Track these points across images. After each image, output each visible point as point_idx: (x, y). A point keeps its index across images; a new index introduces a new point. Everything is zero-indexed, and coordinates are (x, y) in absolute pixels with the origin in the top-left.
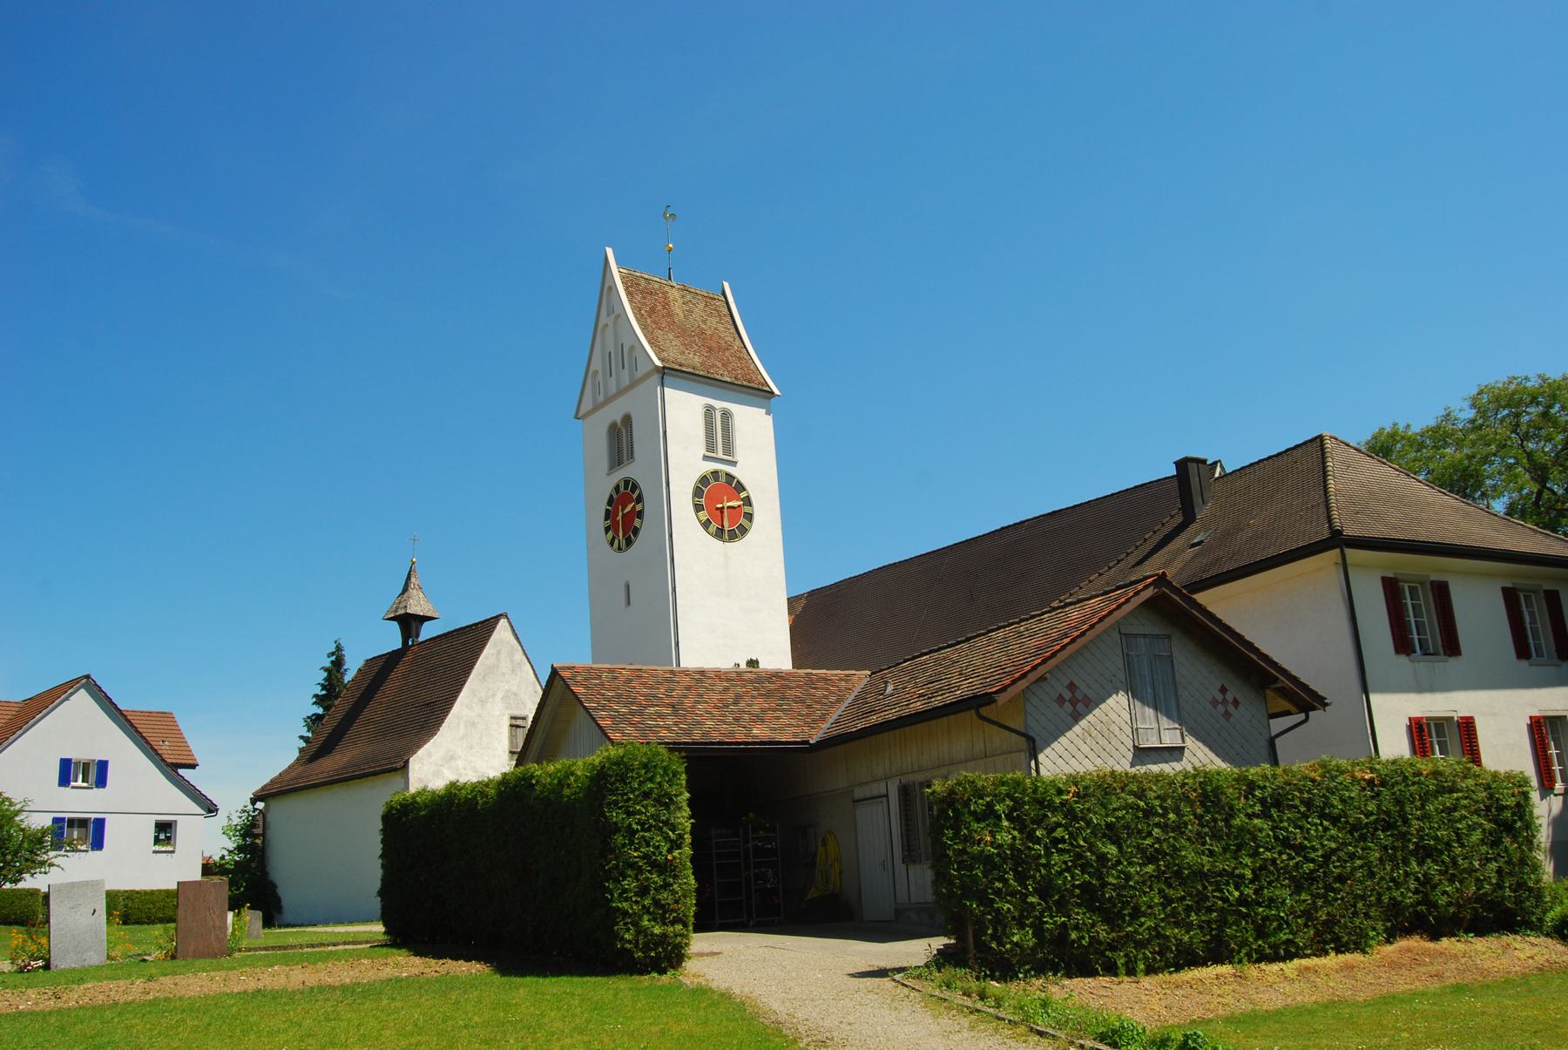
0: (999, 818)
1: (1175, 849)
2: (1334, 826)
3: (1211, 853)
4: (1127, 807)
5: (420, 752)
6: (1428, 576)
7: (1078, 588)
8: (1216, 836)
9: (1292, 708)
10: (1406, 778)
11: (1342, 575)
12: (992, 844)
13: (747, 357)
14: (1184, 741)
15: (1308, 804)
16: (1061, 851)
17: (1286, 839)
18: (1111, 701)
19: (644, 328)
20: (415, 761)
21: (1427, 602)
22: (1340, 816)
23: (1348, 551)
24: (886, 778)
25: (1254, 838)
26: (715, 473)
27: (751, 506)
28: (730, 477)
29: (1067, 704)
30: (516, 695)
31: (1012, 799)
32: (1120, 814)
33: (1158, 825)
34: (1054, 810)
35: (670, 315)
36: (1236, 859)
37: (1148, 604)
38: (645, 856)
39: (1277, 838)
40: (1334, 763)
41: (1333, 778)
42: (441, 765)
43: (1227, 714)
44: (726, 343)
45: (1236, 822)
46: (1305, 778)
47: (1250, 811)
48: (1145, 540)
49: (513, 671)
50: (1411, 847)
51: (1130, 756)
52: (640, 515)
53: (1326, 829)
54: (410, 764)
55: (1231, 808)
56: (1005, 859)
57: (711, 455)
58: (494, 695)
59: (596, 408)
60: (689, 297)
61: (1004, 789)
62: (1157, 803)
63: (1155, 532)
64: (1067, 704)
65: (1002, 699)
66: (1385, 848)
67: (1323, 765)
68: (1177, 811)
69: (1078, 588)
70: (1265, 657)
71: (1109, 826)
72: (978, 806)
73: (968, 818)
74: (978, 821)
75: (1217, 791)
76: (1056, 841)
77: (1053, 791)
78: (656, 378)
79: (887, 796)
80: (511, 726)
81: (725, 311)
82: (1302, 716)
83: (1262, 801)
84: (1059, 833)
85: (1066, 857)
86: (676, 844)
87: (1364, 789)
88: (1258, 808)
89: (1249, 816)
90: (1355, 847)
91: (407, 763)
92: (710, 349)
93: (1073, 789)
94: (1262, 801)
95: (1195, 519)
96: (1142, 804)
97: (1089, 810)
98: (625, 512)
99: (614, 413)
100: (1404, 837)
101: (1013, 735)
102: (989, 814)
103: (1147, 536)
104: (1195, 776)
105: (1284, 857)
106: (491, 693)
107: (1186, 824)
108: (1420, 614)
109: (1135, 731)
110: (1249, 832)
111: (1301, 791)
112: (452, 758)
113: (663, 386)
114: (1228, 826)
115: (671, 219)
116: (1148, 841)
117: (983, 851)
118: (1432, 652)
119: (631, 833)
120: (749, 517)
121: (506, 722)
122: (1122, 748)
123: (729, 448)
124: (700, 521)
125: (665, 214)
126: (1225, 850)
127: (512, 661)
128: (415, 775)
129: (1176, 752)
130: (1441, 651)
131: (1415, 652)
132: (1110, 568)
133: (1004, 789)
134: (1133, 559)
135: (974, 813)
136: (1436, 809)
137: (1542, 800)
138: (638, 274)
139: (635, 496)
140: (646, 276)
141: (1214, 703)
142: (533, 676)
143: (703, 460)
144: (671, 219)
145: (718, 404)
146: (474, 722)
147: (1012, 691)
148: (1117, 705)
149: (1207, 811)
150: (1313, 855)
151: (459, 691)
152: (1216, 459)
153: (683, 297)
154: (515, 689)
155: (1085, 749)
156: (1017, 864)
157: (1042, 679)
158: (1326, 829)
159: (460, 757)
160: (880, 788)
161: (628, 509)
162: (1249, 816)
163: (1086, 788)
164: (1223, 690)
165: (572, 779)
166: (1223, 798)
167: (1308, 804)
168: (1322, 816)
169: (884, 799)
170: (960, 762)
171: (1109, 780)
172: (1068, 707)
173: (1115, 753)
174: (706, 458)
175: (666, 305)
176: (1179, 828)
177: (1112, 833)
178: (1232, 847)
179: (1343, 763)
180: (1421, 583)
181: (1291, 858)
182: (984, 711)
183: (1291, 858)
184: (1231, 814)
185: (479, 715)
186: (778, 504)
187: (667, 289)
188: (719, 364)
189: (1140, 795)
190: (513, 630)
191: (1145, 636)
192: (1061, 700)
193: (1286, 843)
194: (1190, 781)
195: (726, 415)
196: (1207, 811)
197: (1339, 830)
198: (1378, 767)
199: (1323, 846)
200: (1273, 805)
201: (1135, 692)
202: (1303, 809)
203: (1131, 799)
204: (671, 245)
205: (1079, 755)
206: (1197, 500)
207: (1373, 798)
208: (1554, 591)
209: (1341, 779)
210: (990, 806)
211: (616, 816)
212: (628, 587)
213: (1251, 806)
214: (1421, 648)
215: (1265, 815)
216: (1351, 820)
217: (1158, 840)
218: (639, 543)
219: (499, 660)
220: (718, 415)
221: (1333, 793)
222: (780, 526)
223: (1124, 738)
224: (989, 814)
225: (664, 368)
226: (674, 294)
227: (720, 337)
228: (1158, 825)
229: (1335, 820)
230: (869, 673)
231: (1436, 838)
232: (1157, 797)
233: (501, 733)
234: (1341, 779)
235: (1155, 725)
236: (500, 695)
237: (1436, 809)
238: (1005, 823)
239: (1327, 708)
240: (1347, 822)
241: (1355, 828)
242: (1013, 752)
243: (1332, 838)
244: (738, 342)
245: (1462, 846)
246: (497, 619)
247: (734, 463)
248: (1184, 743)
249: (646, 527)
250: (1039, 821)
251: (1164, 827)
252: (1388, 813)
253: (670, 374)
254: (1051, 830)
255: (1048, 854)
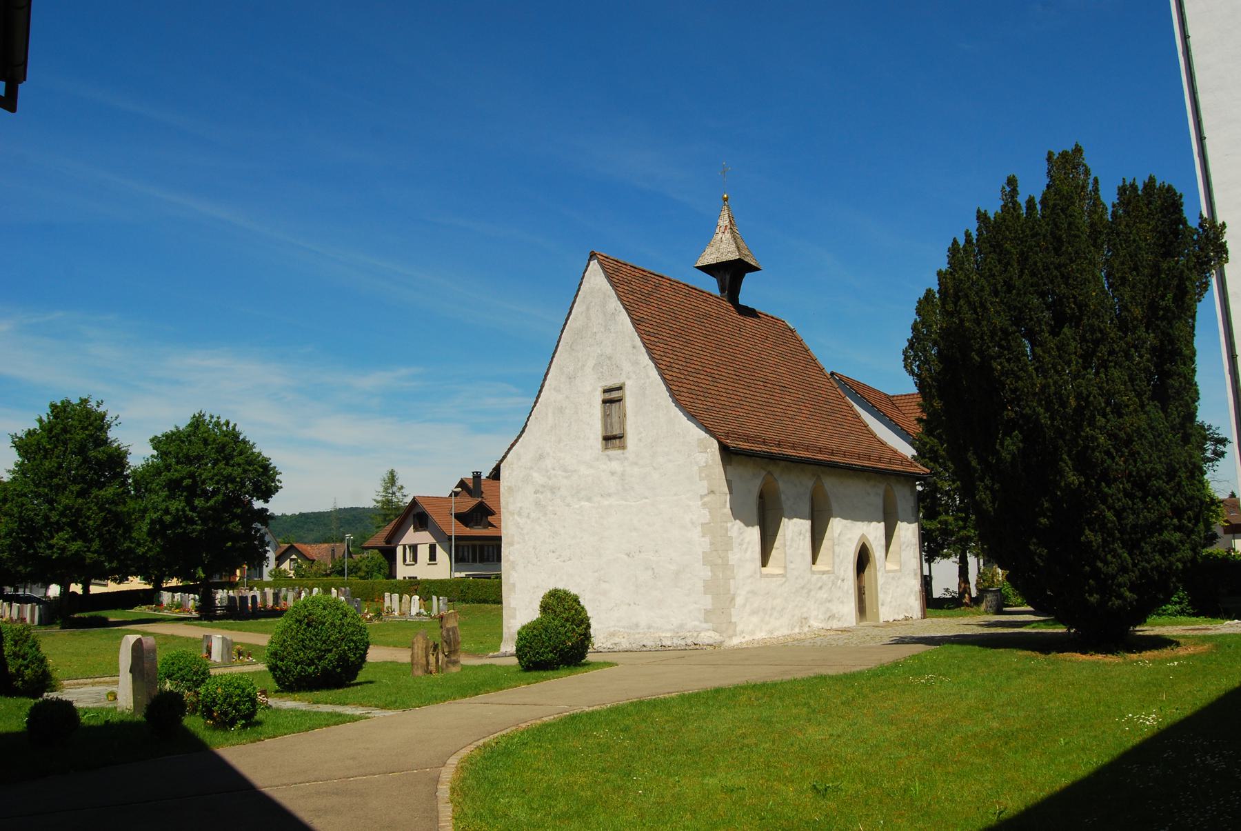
20: (505, 467)
30: (610, 358)
42: (531, 468)
80: (605, 402)
112: (541, 457)
117: (231, 474)
121: (599, 397)
128: (505, 483)
143: (606, 448)
165: (38, 535)
208: (118, 671)
219: (588, 318)
236: (591, 363)
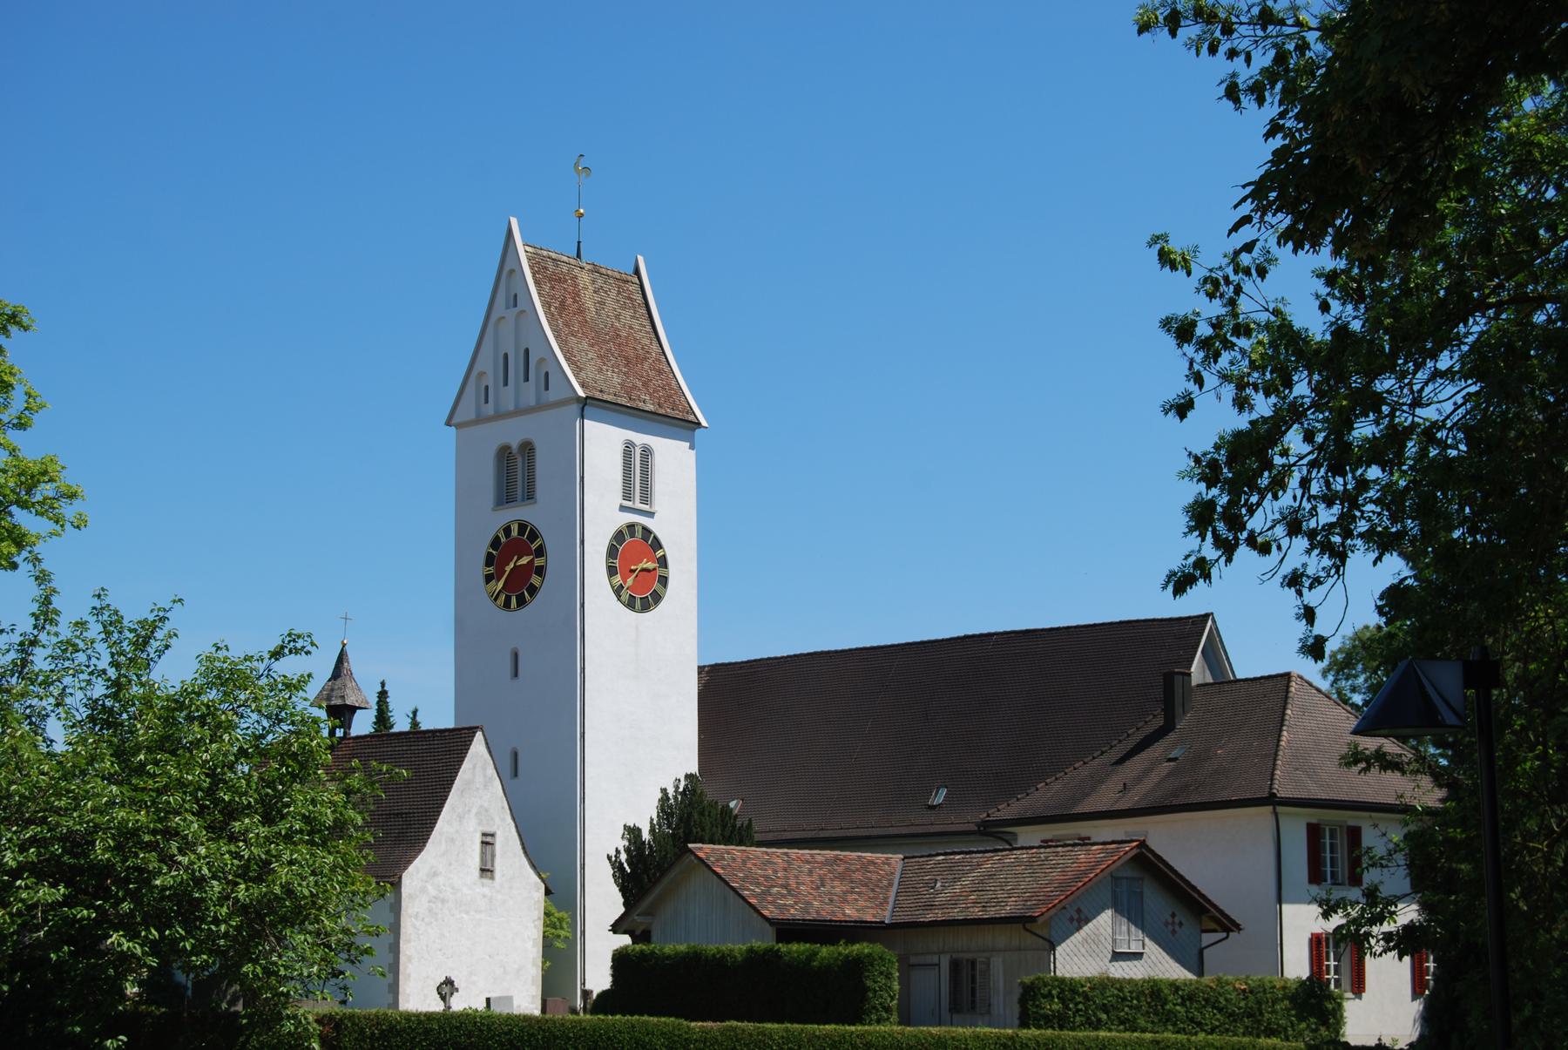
0: (1053, 997)
1: (1135, 1019)
2: (1219, 1012)
3: (1153, 1022)
4: (1113, 996)
5: (411, 868)
6: (1346, 822)
7: (1063, 773)
8: (1156, 1013)
9: (1218, 928)
10: (1265, 990)
11: (1275, 823)
12: (1050, 1010)
13: (667, 369)
14: (1144, 949)
15: (1206, 1000)
16: (1080, 1016)
17: (1193, 1018)
18: (1103, 915)
19: (548, 313)
21: (1342, 842)
22: (1223, 1009)
23: (1280, 809)
24: (940, 953)
25: (1176, 1016)
26: (631, 527)
27: (666, 567)
28: (647, 531)
29: (1075, 922)
31: (1060, 988)
32: (1110, 999)
33: (1128, 1006)
34: (1079, 995)
35: (581, 311)
36: (1165, 1026)
37: (1134, 859)
38: (881, 1004)
39: (1187, 1017)
40: (1225, 978)
41: (1222, 987)
42: (426, 882)
43: (1174, 932)
44: (643, 349)
45: (1168, 1007)
46: (1208, 986)
47: (1175, 1002)
48: (1128, 735)
49: (485, 786)
50: (1263, 1028)
51: (1109, 956)
52: (540, 571)
53: (1215, 1015)
54: (403, 880)
55: (1166, 999)
56: (1054, 1016)
57: (629, 504)
58: (469, 811)
59: (480, 420)
60: (600, 282)
61: (1056, 983)
62: (1128, 994)
63: (1138, 729)
64: (1075, 922)
65: (1041, 920)
66: (1247, 1027)
67: (1219, 980)
68: (1139, 1001)
69: (1063, 773)
70: (1203, 896)
71: (1104, 1005)
72: (1045, 991)
73: (1039, 996)
74: (1044, 998)
75: (1160, 990)
76: (1078, 1010)
77: (1079, 986)
78: (575, 408)
79: (939, 965)
80: (483, 842)
81: (639, 298)
82: (1224, 935)
83: (1182, 997)
84: (1080, 1006)
85: (1083, 1019)
86: (892, 998)
87: (1239, 994)
88: (1179, 1001)
89: (1174, 1005)
90: (1230, 1025)
91: (400, 878)
92: (628, 362)
93: (1089, 985)
94: (1182, 997)
95: (1174, 728)
96: (1121, 994)
97: (1095, 996)
98: (518, 564)
99: (512, 433)
100: (1259, 1022)
101: (1041, 940)
102: (1049, 996)
103: (1130, 732)
104: (1149, 982)
105: (1190, 1027)
106: (467, 808)
107: (1141, 1006)
108: (1336, 855)
109: (1114, 941)
110: (1173, 1013)
111: (1203, 993)
112: (435, 874)
113: (583, 417)
114: (1163, 1009)
115: (584, 174)
116: (1122, 1014)
118: (1340, 881)
119: (875, 991)
120: (664, 581)
121: (478, 839)
122: (1105, 951)
123: (646, 497)
124: (613, 587)
125: (576, 165)
126: (1160, 1021)
127: (485, 776)
129: (1138, 956)
130: (1347, 882)
131: (1326, 881)
132: (1094, 758)
133: (1056, 983)
134: (1115, 754)
135: (1041, 994)
136: (1281, 1009)
137: (1413, 1000)
138: (545, 253)
139: (534, 547)
140: (554, 255)
141: (1167, 924)
142: (501, 791)
143: (620, 510)
144: (584, 174)
145: (639, 439)
146: (453, 839)
147: (1046, 916)
148: (1105, 920)
149: (1153, 1000)
150: (1206, 1028)
151: (441, 806)
152: (1210, 611)
153: (594, 282)
154: (486, 805)
155: (1083, 951)
156: (1059, 1020)
157: (1064, 908)
158: (1215, 1015)
159: (441, 873)
160: (935, 959)
161: (524, 561)
162: (1174, 1005)
163: (1095, 985)
164: (1173, 915)
166: (1162, 994)
167: (1206, 1000)
168: (1214, 1007)
169: (937, 967)
170: (1000, 951)
171: (1106, 981)
172: (1075, 923)
173: (1101, 955)
174: (623, 508)
175: (576, 295)
176: (1138, 1008)
177: (1105, 1009)
178: (250, 750)
179: (1230, 978)
180: (1340, 827)
181: (1193, 1028)
182: (1028, 926)
183: (1193, 1028)
184: (1165, 1002)
185: (457, 832)
186: (695, 564)
187: (576, 271)
188: (639, 384)
189: (1121, 990)
190: (487, 743)
191: (1127, 878)
192: (1072, 919)
193: (1192, 1020)
194: (1146, 984)
195: (647, 452)
196: (1153, 1000)
197: (1222, 1016)
198: (1250, 982)
199: (1212, 1023)
200: (1188, 1000)
201: (1119, 909)
202: (1203, 1003)
203: (1116, 992)
204: (582, 211)
205: (1079, 954)
206: (1179, 710)
207: (1243, 999)
209: (1226, 988)
210: (1050, 991)
211: (869, 983)
212: (516, 656)
213: (1176, 1000)
214: (1332, 877)
215: (1183, 1004)
216: (1230, 1011)
217: (1127, 1014)
218: (536, 605)
220: (638, 451)
221: (1221, 996)
222: (695, 591)
223: (1107, 945)
224: (1049, 996)
225: (587, 398)
226: (584, 278)
227: (635, 339)
228: (1128, 1006)
229: (1220, 1010)
230: (902, 856)
231: (1278, 1024)
232: (1130, 992)
233: (473, 850)
234: (1226, 988)
235: (1127, 938)
236: (474, 810)
237: (1281, 1009)
238: (1056, 1000)
239: (1241, 932)
240: (1226, 1012)
241: (1232, 1014)
242: (1038, 950)
243: (1218, 1020)
244: (655, 346)
245: (1294, 1030)
246: (477, 727)
247: (651, 514)
248: (1144, 949)
249: (548, 587)
250: (1071, 1000)
251: (1130, 1007)
252: (1251, 1008)
253: (590, 405)
254: (1076, 1004)
255: (1074, 1017)
